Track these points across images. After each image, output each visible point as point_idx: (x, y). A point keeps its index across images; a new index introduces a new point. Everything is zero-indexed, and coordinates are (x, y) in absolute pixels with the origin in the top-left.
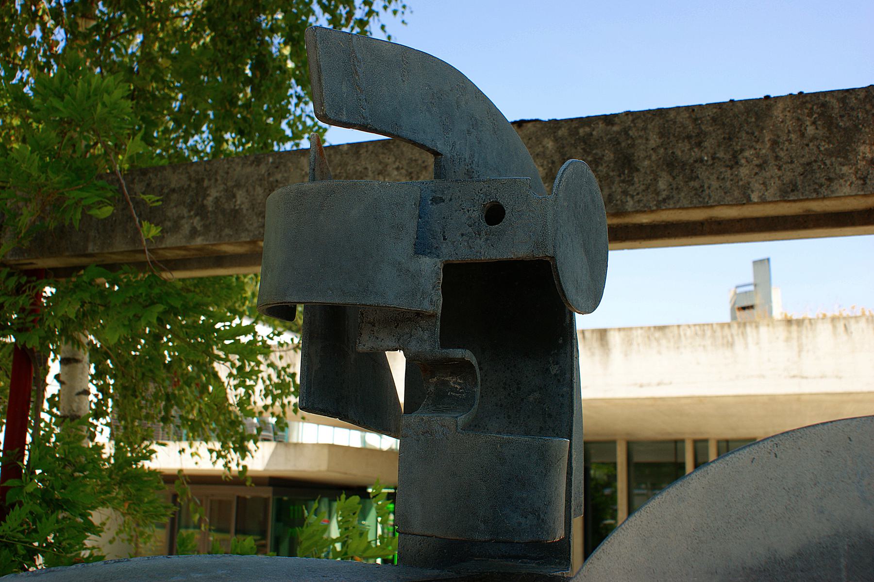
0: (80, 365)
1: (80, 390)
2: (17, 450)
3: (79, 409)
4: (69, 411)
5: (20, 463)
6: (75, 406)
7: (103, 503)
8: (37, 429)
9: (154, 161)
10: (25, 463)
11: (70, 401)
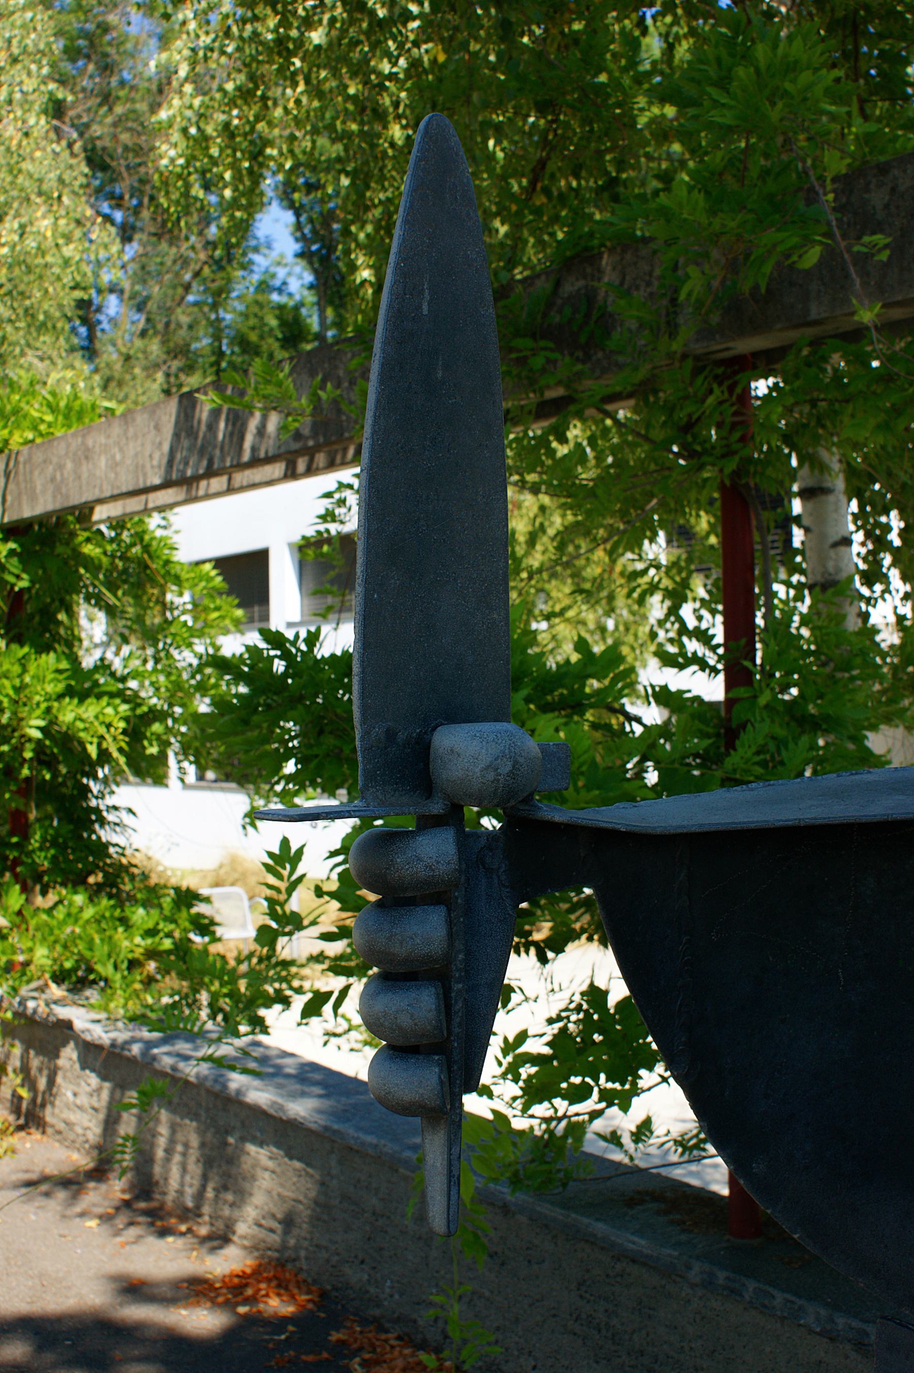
0: (831, 498)
1: (837, 538)
2: (743, 641)
3: (838, 570)
4: (823, 575)
5: (747, 663)
6: (830, 565)
7: (888, 719)
8: (770, 607)
9: (898, 145)
10: (758, 661)
11: (822, 559)
